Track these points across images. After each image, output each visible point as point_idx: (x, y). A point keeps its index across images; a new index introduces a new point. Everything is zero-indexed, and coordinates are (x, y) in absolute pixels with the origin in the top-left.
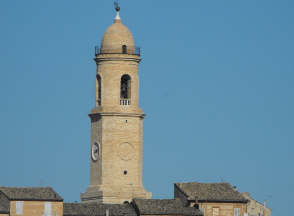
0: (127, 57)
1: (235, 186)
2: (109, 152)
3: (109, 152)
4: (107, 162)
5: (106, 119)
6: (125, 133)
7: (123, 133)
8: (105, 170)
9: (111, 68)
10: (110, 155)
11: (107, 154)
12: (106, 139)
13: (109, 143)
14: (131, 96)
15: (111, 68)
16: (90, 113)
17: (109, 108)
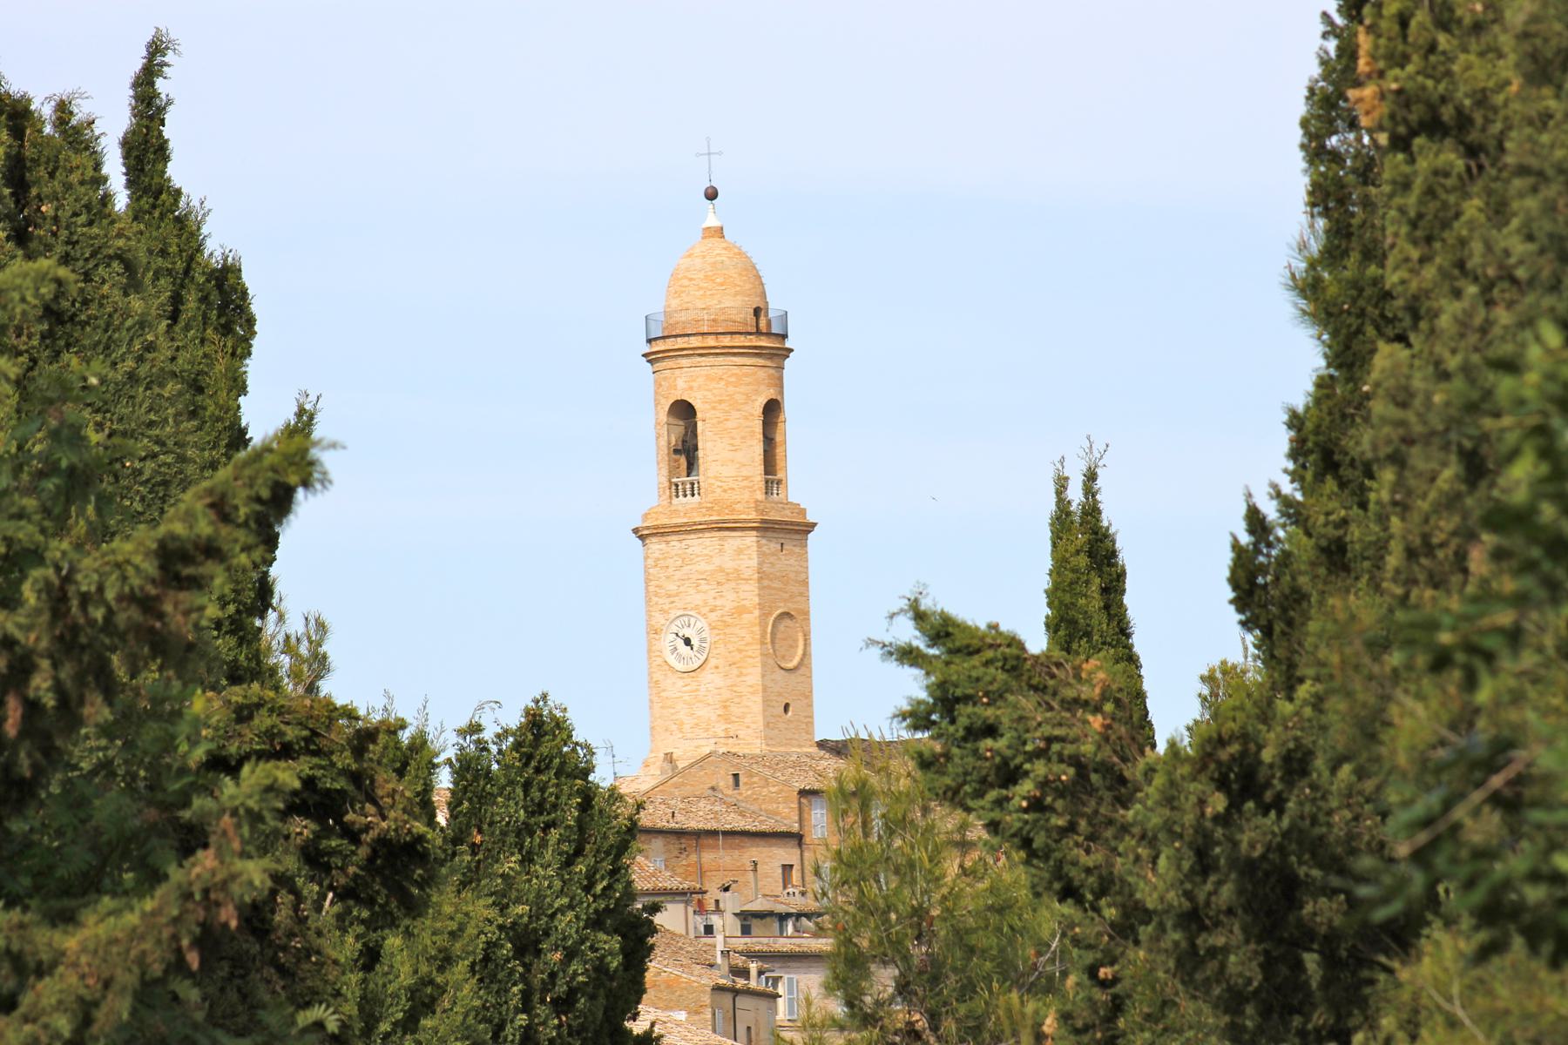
0: (662, 348)
1: (327, 618)
2: (747, 645)
3: (747, 645)
4: (741, 674)
5: (730, 540)
6: (780, 585)
7: (776, 584)
8: (736, 700)
9: (733, 379)
10: (750, 653)
11: (740, 651)
12: (736, 604)
13: (745, 616)
14: (701, 461)
15: (733, 379)
16: (639, 524)
17: (738, 507)
